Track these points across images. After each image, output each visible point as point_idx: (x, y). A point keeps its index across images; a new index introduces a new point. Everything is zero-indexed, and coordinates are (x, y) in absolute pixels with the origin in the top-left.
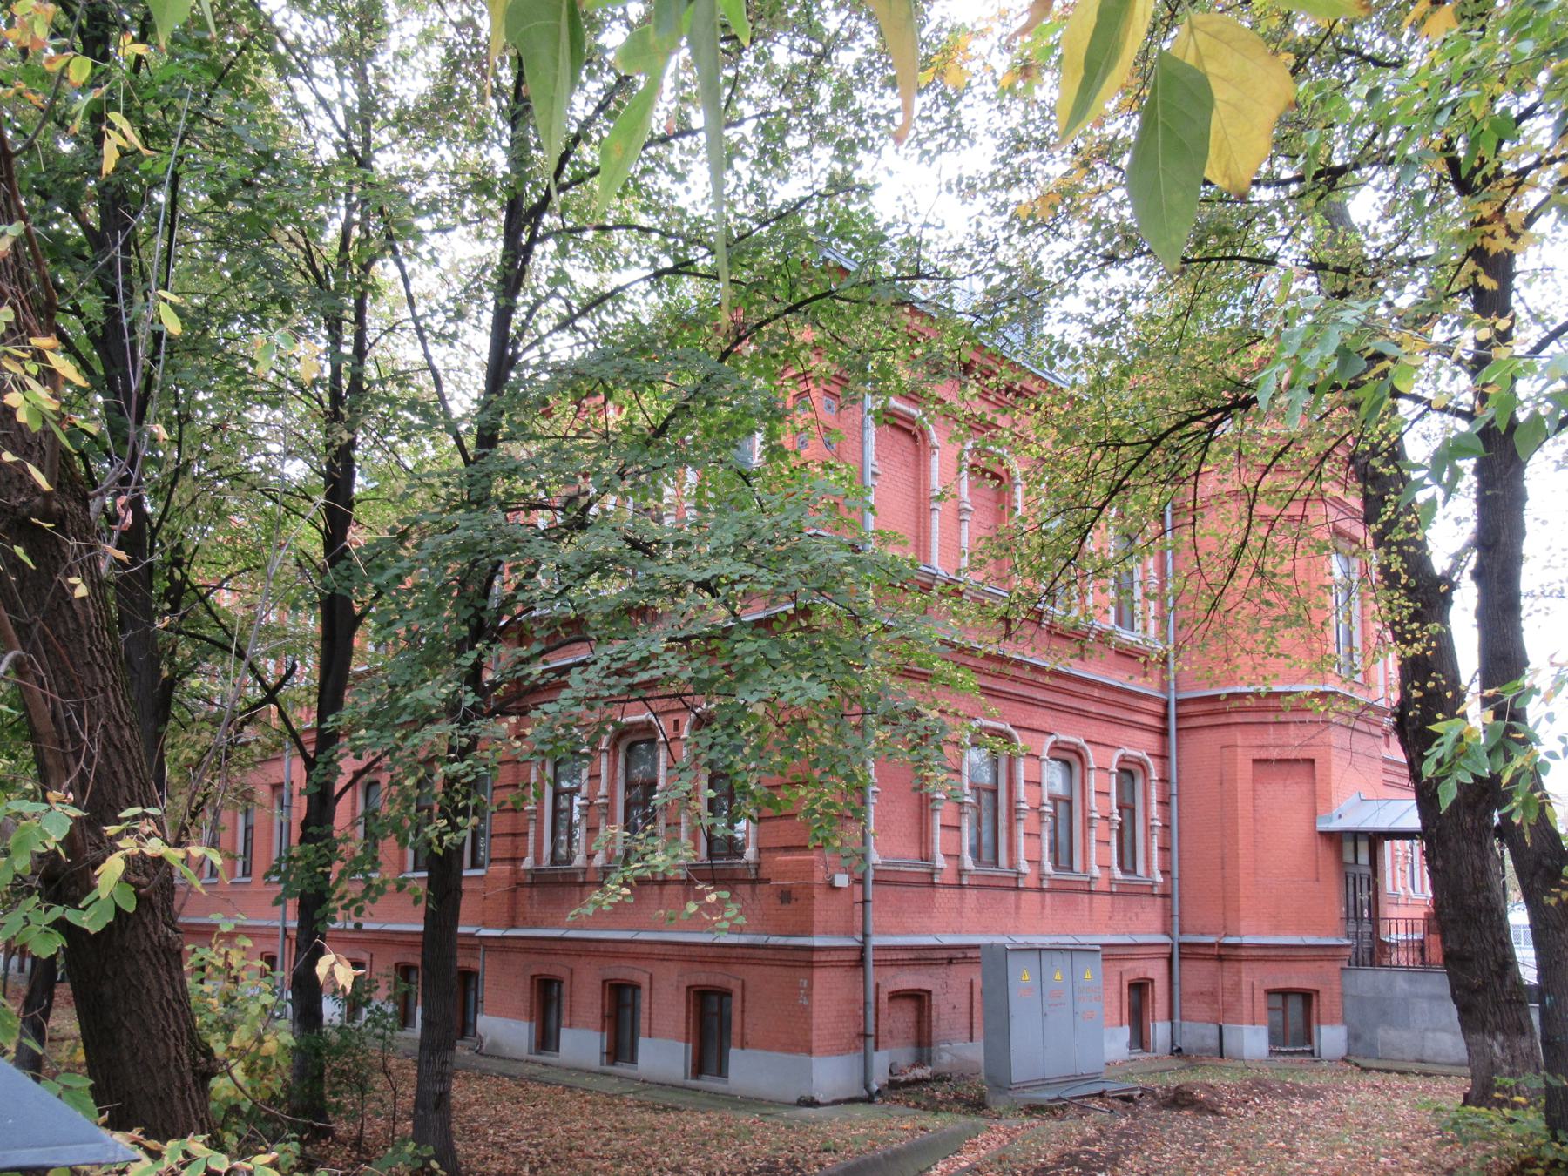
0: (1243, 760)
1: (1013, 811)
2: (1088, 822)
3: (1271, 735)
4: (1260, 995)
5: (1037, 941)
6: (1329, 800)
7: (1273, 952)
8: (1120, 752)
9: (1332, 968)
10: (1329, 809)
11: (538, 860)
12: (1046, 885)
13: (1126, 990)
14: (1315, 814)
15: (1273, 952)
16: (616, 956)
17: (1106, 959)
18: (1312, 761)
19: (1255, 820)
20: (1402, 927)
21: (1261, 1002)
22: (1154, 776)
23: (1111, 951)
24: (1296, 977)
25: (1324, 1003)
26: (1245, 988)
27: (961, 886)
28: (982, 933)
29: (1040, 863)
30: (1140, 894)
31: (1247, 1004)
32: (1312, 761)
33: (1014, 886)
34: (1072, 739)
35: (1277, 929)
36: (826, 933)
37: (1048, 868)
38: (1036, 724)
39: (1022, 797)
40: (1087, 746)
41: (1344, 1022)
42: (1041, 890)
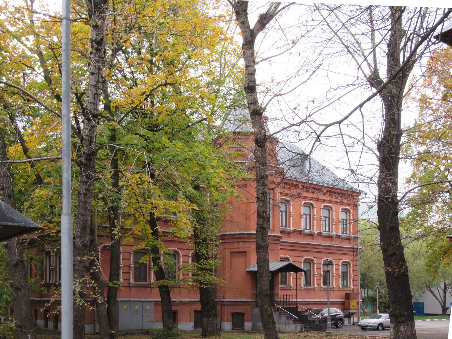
0: (228, 252)
1: (314, 275)
2: (314, 276)
3: (235, 245)
4: (229, 314)
5: (143, 300)
6: (250, 263)
7: (232, 303)
8: (342, 261)
9: (249, 307)
10: (250, 265)
11: (46, 281)
12: (131, 286)
13: (193, 313)
14: (246, 266)
15: (232, 303)
16: (309, 304)
17: (155, 305)
18: (246, 252)
19: (231, 268)
20: (291, 297)
21: (230, 317)
22: (352, 265)
23: (157, 303)
24: (239, 310)
25: (246, 316)
26: (226, 312)
27: (130, 287)
28: (137, 298)
29: (339, 285)
30: (142, 287)
31: (226, 317)
32: (246, 252)
33: (314, 289)
34: (310, 258)
35: (235, 297)
36: (332, 299)
37: (341, 286)
38: (337, 258)
39: (334, 273)
40: (179, 250)
41: (252, 321)
42: (130, 287)
